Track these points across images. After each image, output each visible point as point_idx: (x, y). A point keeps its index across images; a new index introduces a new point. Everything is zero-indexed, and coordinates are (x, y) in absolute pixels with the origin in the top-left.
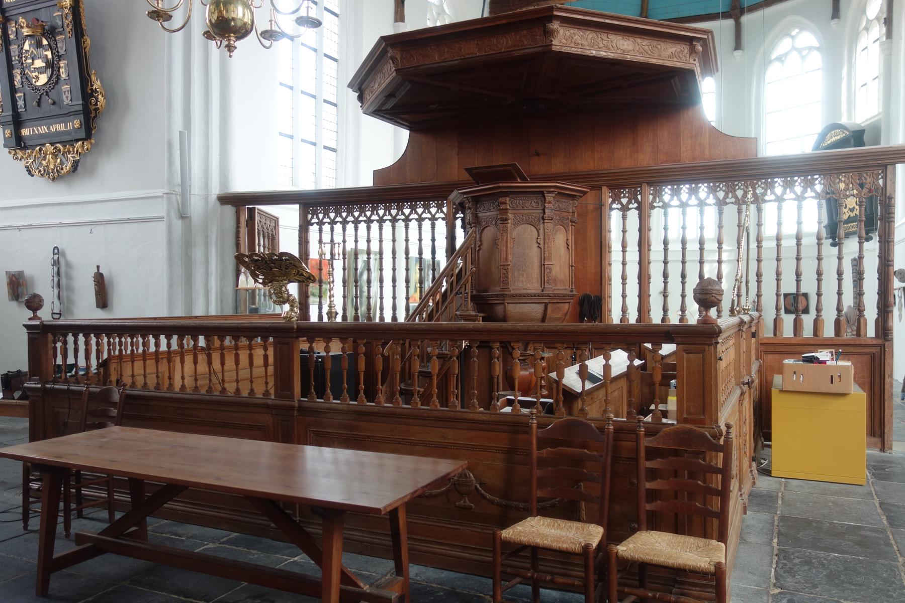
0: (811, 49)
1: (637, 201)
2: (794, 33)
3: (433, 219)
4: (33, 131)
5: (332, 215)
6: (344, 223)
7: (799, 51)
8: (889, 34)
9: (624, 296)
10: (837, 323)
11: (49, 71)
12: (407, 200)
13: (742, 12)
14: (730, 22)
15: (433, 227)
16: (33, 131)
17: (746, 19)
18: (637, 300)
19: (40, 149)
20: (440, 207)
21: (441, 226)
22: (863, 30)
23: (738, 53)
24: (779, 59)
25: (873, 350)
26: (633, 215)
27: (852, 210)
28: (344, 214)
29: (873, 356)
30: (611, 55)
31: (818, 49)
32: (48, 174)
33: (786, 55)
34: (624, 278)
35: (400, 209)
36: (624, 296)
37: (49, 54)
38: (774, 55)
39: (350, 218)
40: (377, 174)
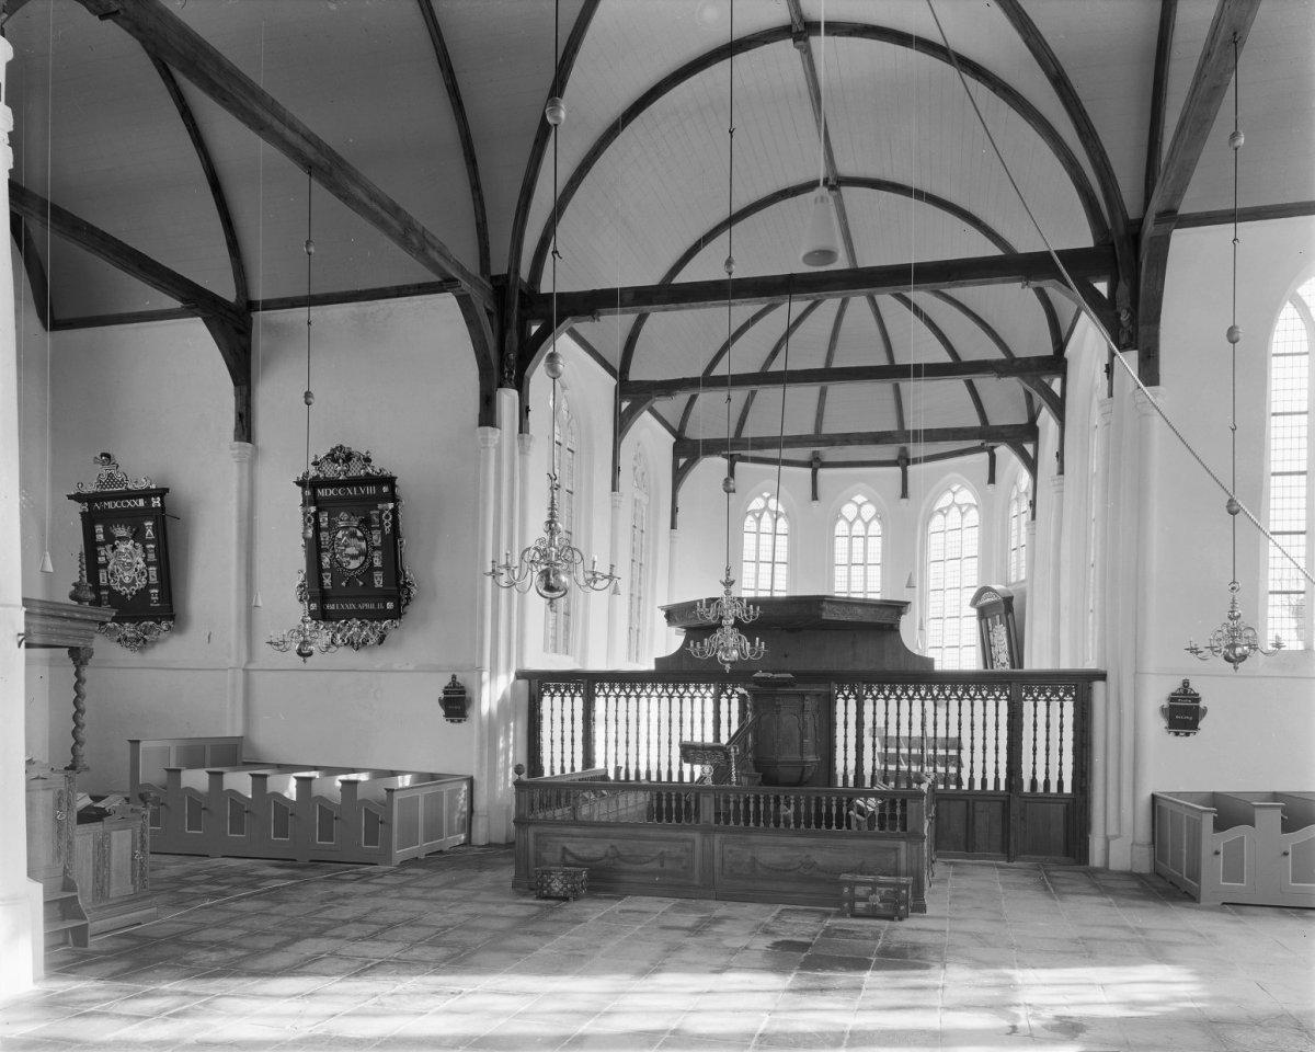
0: (970, 506)
1: (854, 693)
2: (955, 488)
3: (703, 697)
4: (340, 606)
5: (617, 690)
6: (628, 697)
7: (960, 507)
8: (1034, 517)
9: (846, 759)
10: (873, 777)
11: (362, 559)
12: (683, 682)
13: (908, 462)
14: (898, 470)
15: (703, 702)
16: (340, 606)
17: (911, 469)
18: (854, 762)
19: (346, 622)
20: (708, 688)
21: (709, 704)
22: (1033, 418)
23: (904, 500)
24: (941, 511)
25: (1003, 798)
26: (852, 703)
27: (1003, 665)
28: (628, 690)
29: (1004, 802)
30: (854, 619)
31: (976, 507)
32: (353, 644)
33: (949, 508)
34: (846, 746)
35: (676, 688)
36: (846, 759)
37: (363, 545)
38: (937, 508)
39: (633, 693)
40: (658, 661)
